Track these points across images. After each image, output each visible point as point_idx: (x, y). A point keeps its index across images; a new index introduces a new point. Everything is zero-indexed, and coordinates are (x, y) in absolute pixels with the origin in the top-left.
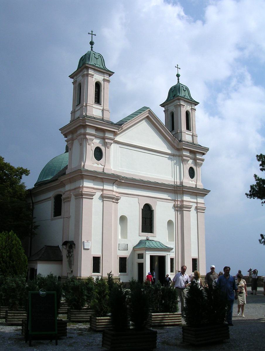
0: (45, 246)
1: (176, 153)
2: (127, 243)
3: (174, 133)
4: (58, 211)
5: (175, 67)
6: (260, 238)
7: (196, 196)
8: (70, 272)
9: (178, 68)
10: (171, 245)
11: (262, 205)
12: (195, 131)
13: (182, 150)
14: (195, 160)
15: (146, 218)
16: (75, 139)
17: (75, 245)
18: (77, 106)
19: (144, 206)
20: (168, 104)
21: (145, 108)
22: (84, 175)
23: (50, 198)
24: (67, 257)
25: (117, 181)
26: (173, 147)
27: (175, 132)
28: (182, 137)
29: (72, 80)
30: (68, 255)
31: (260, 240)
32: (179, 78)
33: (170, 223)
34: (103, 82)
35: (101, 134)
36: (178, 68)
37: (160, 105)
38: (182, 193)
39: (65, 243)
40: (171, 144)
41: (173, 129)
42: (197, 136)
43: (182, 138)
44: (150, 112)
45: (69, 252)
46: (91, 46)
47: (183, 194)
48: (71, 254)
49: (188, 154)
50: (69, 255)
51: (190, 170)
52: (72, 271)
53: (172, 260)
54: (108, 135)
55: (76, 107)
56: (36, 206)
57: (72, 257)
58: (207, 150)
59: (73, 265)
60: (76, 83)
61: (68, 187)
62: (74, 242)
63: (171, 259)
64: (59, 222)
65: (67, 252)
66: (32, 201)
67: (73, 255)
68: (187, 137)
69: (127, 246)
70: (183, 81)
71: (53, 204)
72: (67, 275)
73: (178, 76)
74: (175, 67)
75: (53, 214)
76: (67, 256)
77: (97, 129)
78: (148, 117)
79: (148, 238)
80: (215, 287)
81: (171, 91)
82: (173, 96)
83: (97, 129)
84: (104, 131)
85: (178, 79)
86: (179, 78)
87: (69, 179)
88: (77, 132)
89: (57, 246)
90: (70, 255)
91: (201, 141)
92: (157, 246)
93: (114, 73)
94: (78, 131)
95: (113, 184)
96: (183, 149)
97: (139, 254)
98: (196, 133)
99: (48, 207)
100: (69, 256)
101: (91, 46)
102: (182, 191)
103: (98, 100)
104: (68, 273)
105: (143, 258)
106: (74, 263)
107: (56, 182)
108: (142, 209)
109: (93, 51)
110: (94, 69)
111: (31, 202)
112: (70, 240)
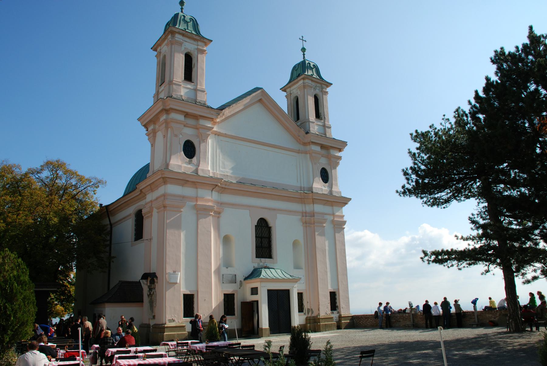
0: (119, 281)
1: (301, 148)
2: (235, 274)
3: (299, 124)
4: (139, 234)
5: (300, 38)
6: (423, 255)
7: (332, 206)
8: (152, 317)
9: (303, 40)
10: (297, 273)
11: (423, 206)
12: (328, 121)
13: (310, 145)
14: (329, 157)
15: (261, 238)
16: (158, 131)
17: (157, 277)
18: (160, 86)
19: (258, 221)
20: (290, 87)
21: (257, 89)
22: (167, 179)
23: (130, 215)
24: (148, 296)
25: (217, 187)
26: (297, 141)
27: (300, 122)
28: (310, 128)
29: (155, 53)
30: (149, 294)
31: (422, 258)
32: (305, 53)
33: (295, 244)
34: (196, 53)
35: (191, 122)
36: (303, 40)
37: (280, 89)
38: (312, 203)
39: (145, 276)
40: (297, 139)
41: (298, 118)
42: (330, 127)
43: (310, 129)
44: (264, 93)
45: (150, 289)
46: (181, 7)
47: (313, 204)
48: (153, 291)
49: (318, 149)
50: (150, 293)
51: (323, 172)
52: (154, 317)
53: (300, 295)
54: (202, 122)
55: (159, 87)
56: (115, 229)
57: (153, 295)
58: (344, 144)
59: (155, 307)
60: (160, 56)
61: (150, 197)
62: (156, 274)
63: (298, 293)
64: (141, 245)
65: (148, 289)
66: (110, 221)
67: (154, 293)
68: (315, 128)
69: (234, 277)
70: (310, 58)
71: (134, 223)
72: (149, 322)
73: (303, 50)
74: (300, 38)
75: (134, 237)
76: (148, 295)
77: (187, 115)
78: (260, 101)
79: (265, 266)
80: (522, 239)
81: (294, 70)
82: (298, 75)
83: (187, 115)
84: (196, 117)
85: (304, 55)
86: (305, 53)
87: (150, 185)
88: (160, 120)
89: (138, 281)
90: (152, 293)
91: (336, 133)
92: (278, 276)
93: (212, 41)
94: (160, 119)
95: (212, 191)
96: (311, 143)
97: (252, 289)
98: (329, 123)
99: (129, 226)
100: (150, 294)
101: (181, 7)
102: (312, 200)
103: (189, 76)
104: (149, 319)
105: (258, 294)
106: (156, 304)
107: (135, 192)
108: (256, 226)
109: (183, 13)
110: (183, 35)
111: (108, 223)
112: (151, 272)
